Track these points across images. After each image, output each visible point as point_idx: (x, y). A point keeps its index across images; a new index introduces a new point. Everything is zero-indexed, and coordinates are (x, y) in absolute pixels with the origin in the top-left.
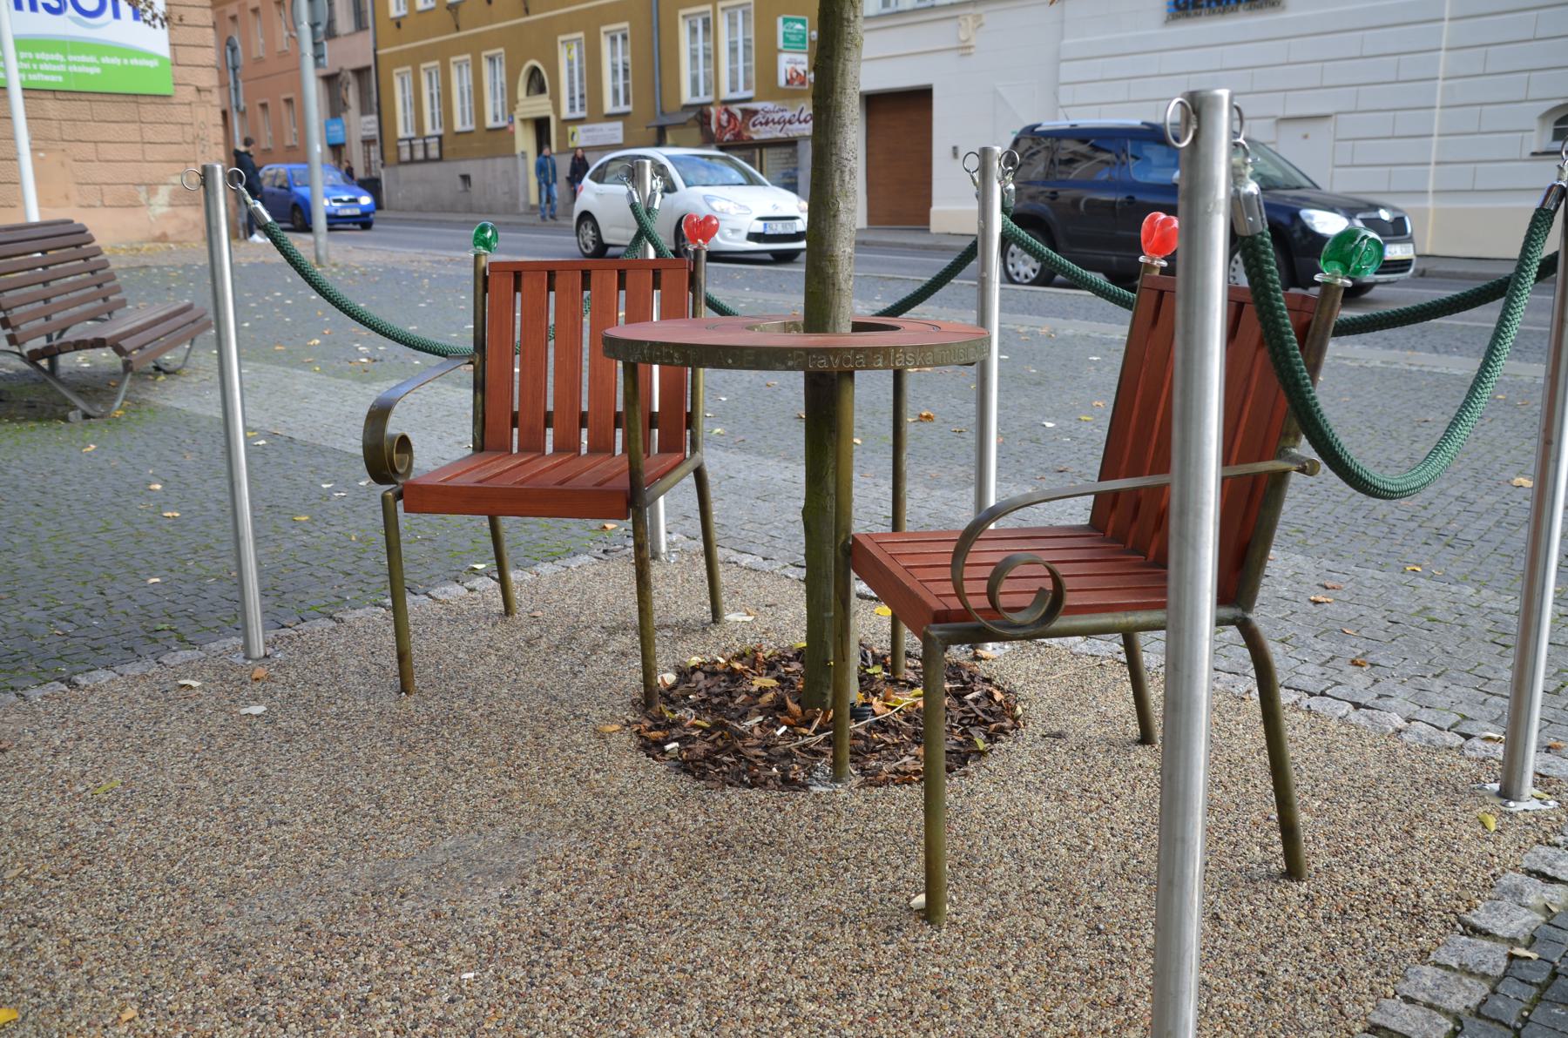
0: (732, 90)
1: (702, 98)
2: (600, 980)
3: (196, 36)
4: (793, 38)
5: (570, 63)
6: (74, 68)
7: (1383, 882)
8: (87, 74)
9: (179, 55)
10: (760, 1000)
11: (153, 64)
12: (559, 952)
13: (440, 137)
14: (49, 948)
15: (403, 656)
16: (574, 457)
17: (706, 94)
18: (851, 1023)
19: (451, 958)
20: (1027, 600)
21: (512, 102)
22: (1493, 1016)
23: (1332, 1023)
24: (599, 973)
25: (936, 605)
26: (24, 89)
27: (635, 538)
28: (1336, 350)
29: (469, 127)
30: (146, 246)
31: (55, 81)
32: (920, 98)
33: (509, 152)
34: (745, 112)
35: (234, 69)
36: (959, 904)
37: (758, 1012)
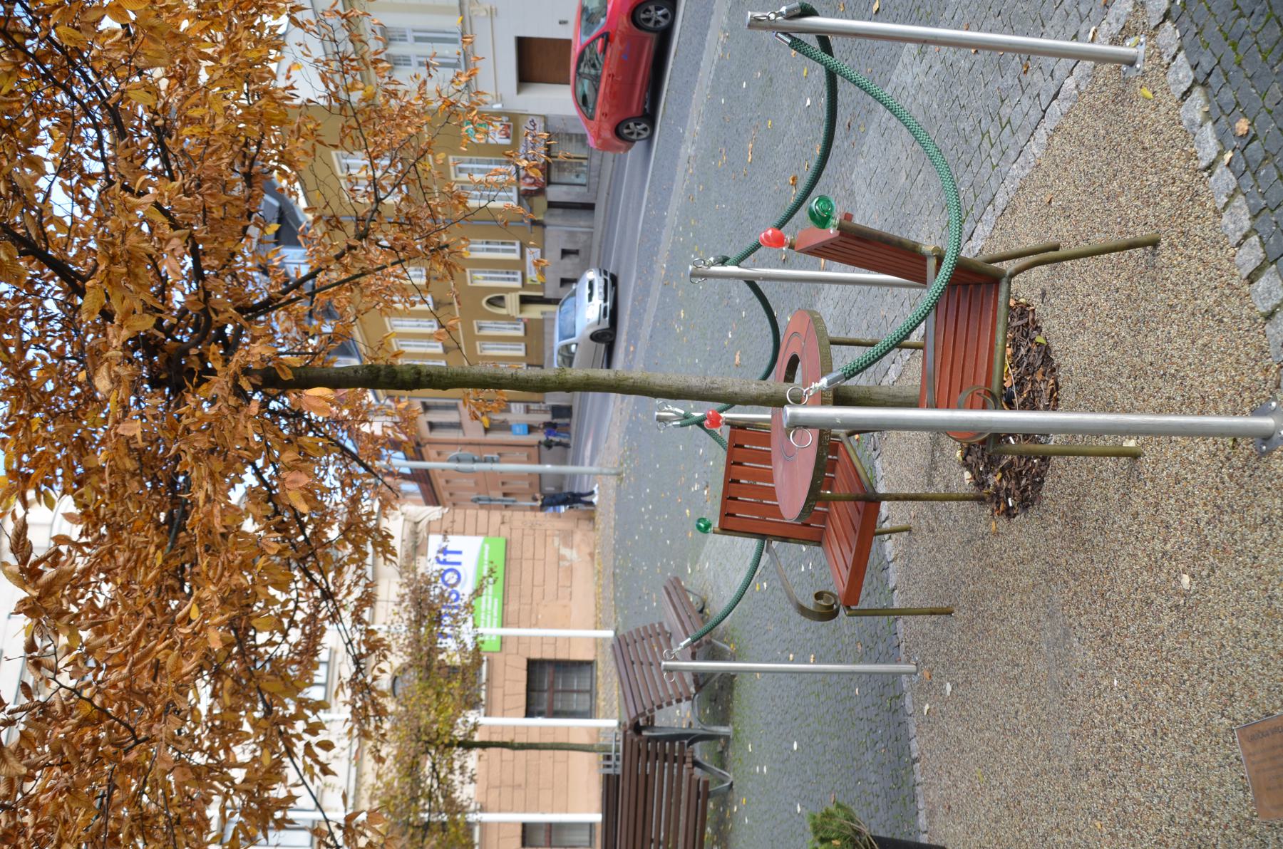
2: (1132, 629)
3: (470, 521)
5: (486, 278)
11: (487, 547)
13: (528, 365)
14: (1059, 838)
15: (932, 613)
21: (509, 318)
24: (1128, 626)
29: (523, 347)
30: (596, 565)
32: (525, 46)
33: (541, 323)
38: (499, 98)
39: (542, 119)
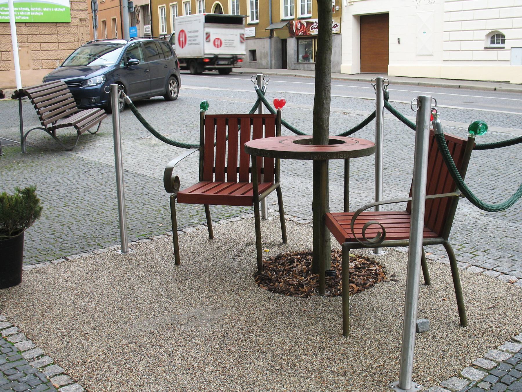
0: (302, 14)
1: (289, 17)
6: (33, 13)
7: (491, 327)
10: (289, 355)
11: (63, 10)
12: (229, 341)
16: (234, 184)
17: (291, 15)
18: (316, 361)
19: (197, 342)
20: (375, 235)
22: (509, 363)
23: (461, 364)
25: (347, 237)
26: (16, 23)
27: (255, 210)
31: (26, 19)
34: (308, 23)
35: (95, 11)
36: (355, 331)
37: (288, 358)
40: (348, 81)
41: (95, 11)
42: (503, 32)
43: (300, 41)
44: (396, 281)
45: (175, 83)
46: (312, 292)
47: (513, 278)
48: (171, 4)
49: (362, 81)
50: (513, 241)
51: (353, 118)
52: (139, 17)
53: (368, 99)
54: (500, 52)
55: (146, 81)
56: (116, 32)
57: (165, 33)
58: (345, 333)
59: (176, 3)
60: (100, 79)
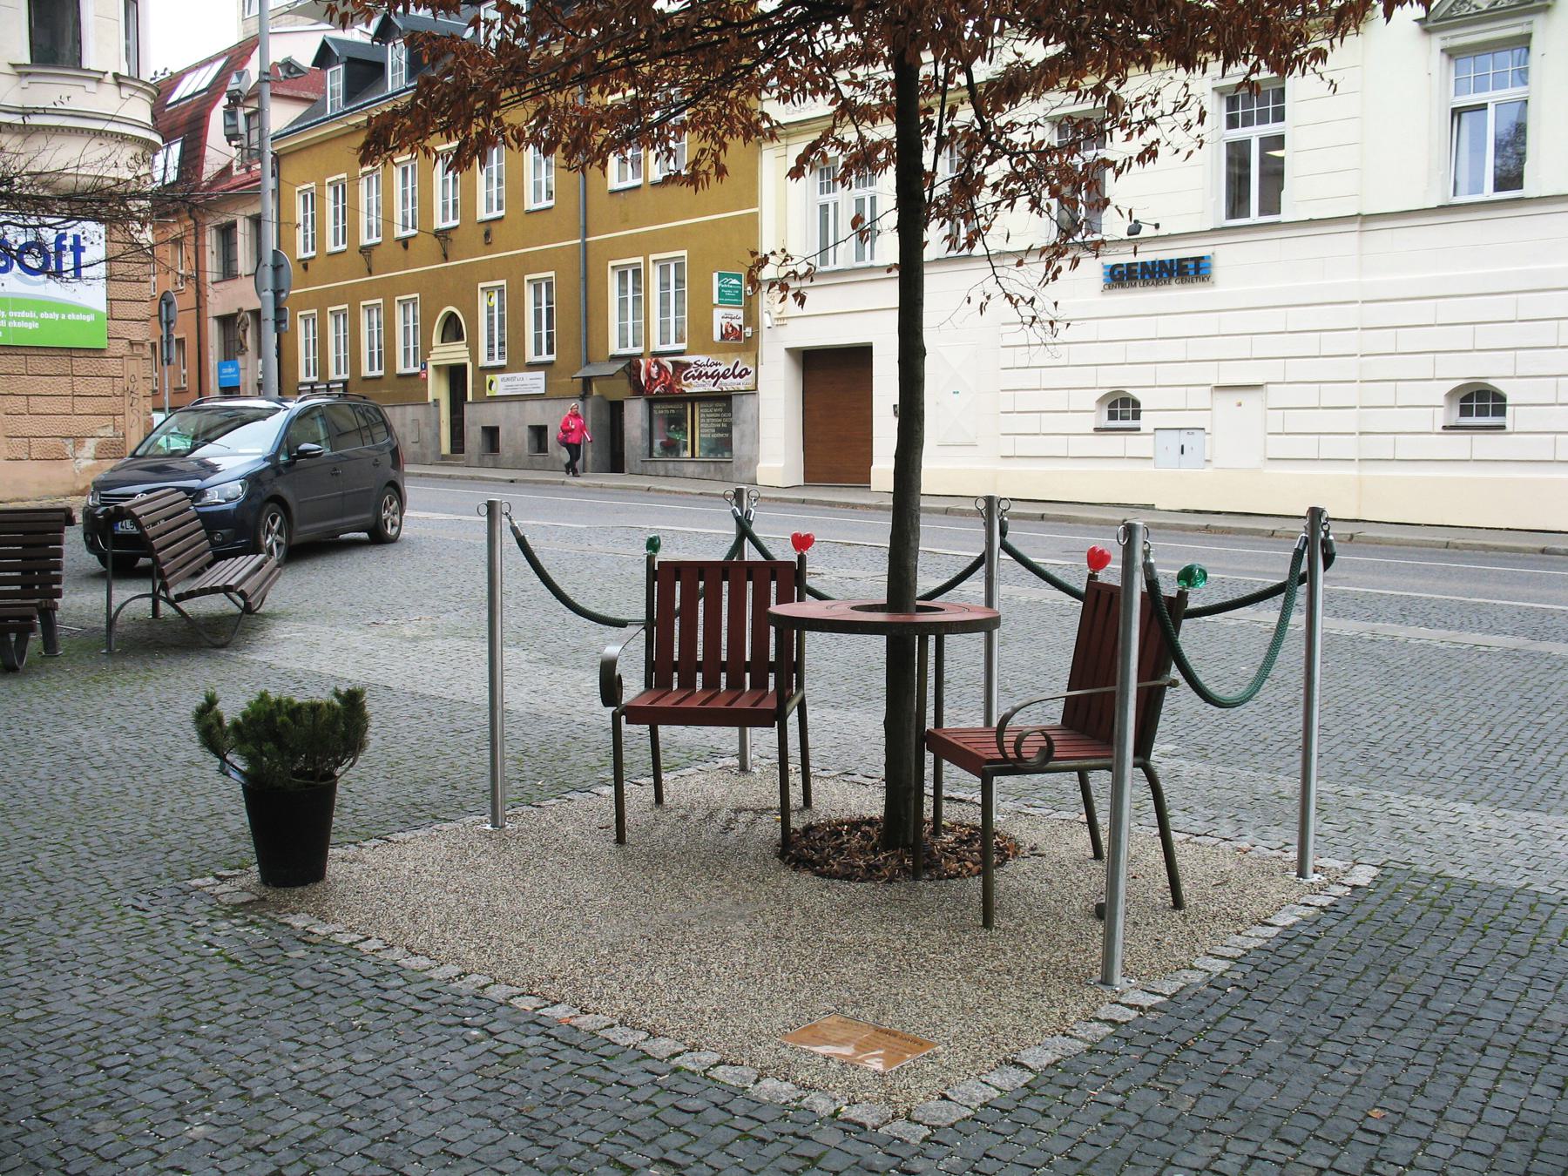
4: (728, 293)
5: (490, 310)
6: (13, 324)
8: (27, 329)
9: (115, 310)
11: (89, 318)
13: (345, 382)
17: (635, 345)
28: (1185, 622)
33: (421, 400)
35: (168, 324)
36: (999, 920)
38: (782, 320)
39: (750, 387)
40: (778, 503)
41: (168, 324)
42: (1136, 394)
43: (657, 407)
44: (1040, 855)
45: (395, 503)
46: (899, 876)
47: (1246, 845)
48: (330, 309)
49: (812, 502)
50: (1231, 794)
51: (833, 584)
52: (245, 337)
53: (849, 544)
54: (1131, 439)
55: (335, 497)
56: (185, 371)
57: (313, 379)
58: (987, 923)
59: (346, 306)
60: (236, 489)
